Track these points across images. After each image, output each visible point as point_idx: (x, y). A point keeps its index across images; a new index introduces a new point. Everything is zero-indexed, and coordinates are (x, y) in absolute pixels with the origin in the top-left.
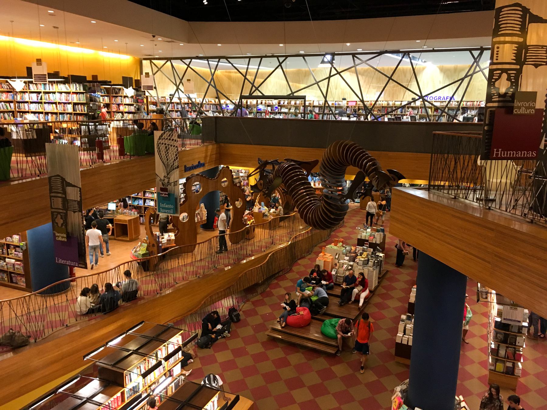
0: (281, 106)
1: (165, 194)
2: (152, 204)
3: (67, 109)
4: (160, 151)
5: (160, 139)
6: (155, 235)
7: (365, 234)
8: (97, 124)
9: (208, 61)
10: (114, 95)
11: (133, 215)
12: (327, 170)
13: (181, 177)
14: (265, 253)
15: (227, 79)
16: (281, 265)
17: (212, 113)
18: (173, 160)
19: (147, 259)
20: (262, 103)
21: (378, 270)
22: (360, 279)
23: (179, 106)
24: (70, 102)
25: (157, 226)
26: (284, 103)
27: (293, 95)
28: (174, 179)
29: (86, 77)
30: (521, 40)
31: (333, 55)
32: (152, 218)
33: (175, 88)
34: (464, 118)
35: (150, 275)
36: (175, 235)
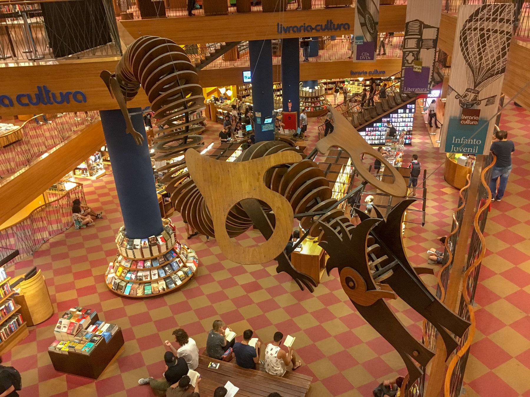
4: (466, 44)
5: (470, 20)
18: (495, 58)
30: (420, 37)
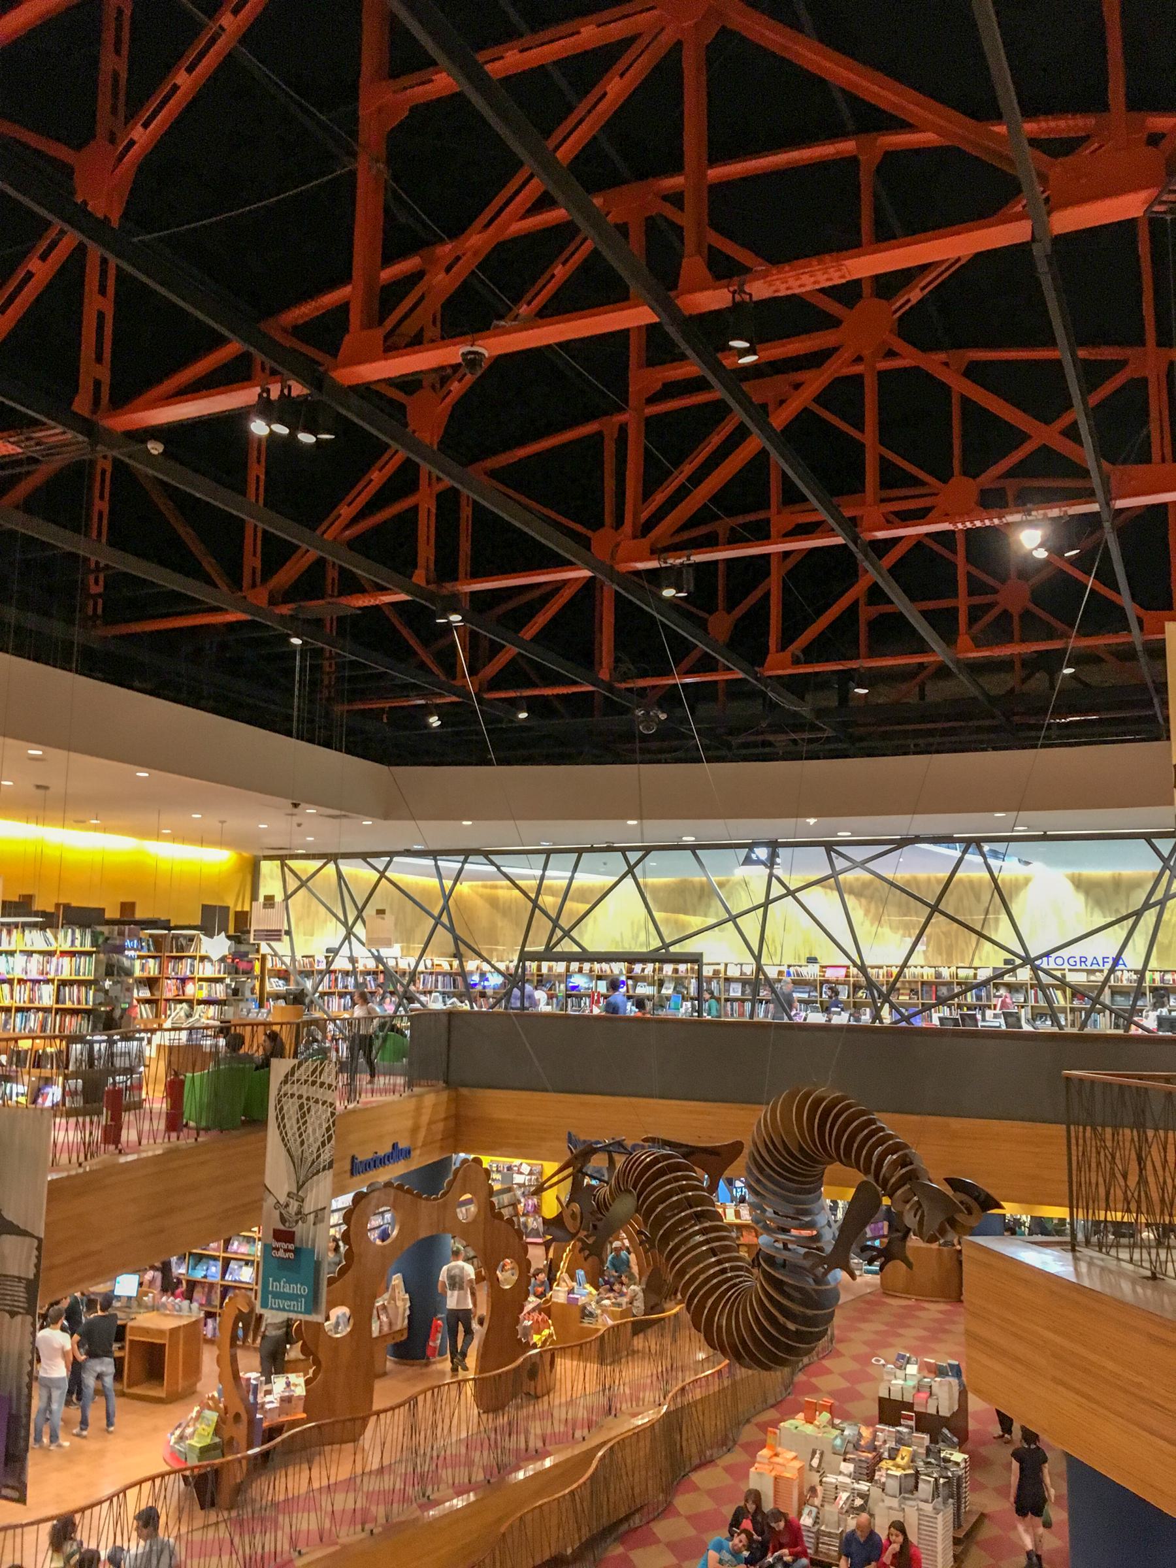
0: (636, 979)
1: (286, 1251)
2: (246, 1274)
3: (40, 998)
4: (283, 1118)
5: (285, 1082)
6: (243, 1383)
7: (901, 1382)
8: (116, 1037)
9: (436, 861)
10: (174, 954)
11: (185, 1313)
12: (769, 1178)
13: (338, 1191)
14: (584, 1447)
15: (488, 906)
16: (637, 1491)
17: (440, 998)
18: (319, 1143)
19: (211, 1465)
20: (580, 970)
21: (950, 1510)
22: (895, 1547)
23: (351, 981)
24: (49, 977)
25: (255, 1349)
26: (643, 970)
27: (667, 951)
28: (316, 1203)
29: (103, 910)
31: (774, 846)
32: (240, 1325)
33: (342, 931)
34: (1161, 1021)
35: (217, 1523)
36: (307, 1382)
